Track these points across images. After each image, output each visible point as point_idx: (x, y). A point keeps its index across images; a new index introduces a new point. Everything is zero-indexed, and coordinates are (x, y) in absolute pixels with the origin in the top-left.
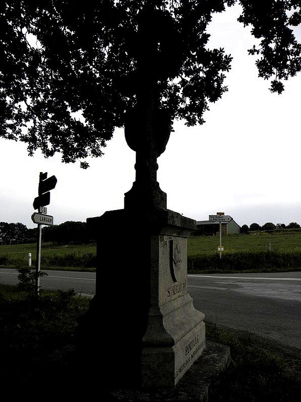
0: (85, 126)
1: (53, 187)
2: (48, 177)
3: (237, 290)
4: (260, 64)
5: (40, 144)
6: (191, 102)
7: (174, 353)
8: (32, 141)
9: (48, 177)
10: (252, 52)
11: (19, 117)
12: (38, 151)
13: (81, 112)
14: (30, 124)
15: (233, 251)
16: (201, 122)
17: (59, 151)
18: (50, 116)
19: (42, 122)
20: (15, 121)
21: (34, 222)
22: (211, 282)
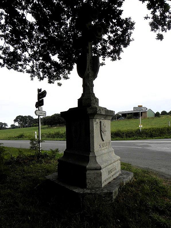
0: (59, 63)
1: (45, 96)
2: (42, 91)
3: (146, 148)
4: (152, 24)
5: (37, 74)
6: (113, 48)
7: (101, 173)
8: (32, 72)
9: (42, 91)
10: (146, 18)
11: (25, 60)
12: (36, 78)
13: (57, 55)
14: (31, 64)
15: (148, 127)
16: (119, 59)
17: (46, 77)
18: (41, 58)
19: (37, 62)
20: (23, 63)
21: (36, 115)
22: (134, 144)
